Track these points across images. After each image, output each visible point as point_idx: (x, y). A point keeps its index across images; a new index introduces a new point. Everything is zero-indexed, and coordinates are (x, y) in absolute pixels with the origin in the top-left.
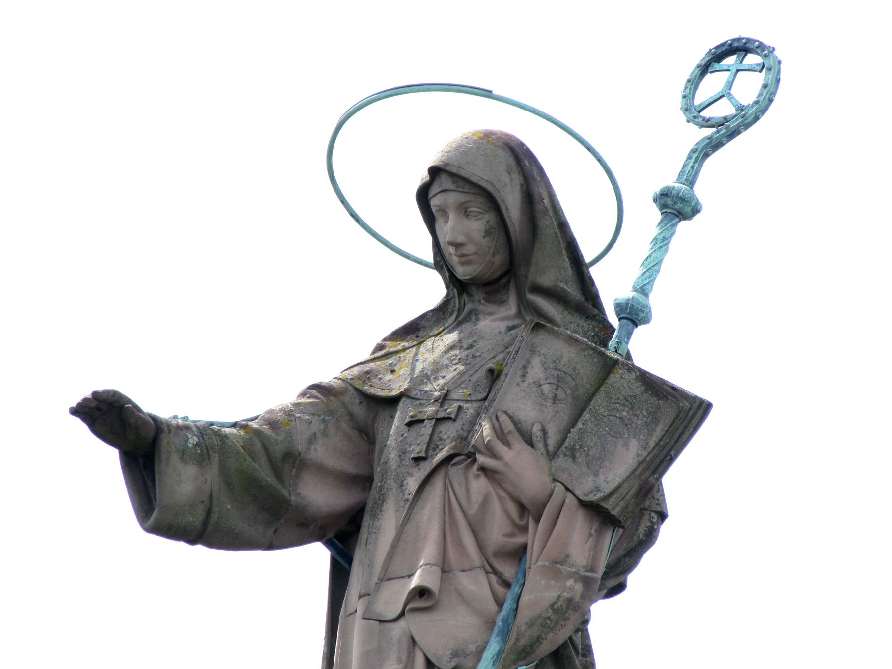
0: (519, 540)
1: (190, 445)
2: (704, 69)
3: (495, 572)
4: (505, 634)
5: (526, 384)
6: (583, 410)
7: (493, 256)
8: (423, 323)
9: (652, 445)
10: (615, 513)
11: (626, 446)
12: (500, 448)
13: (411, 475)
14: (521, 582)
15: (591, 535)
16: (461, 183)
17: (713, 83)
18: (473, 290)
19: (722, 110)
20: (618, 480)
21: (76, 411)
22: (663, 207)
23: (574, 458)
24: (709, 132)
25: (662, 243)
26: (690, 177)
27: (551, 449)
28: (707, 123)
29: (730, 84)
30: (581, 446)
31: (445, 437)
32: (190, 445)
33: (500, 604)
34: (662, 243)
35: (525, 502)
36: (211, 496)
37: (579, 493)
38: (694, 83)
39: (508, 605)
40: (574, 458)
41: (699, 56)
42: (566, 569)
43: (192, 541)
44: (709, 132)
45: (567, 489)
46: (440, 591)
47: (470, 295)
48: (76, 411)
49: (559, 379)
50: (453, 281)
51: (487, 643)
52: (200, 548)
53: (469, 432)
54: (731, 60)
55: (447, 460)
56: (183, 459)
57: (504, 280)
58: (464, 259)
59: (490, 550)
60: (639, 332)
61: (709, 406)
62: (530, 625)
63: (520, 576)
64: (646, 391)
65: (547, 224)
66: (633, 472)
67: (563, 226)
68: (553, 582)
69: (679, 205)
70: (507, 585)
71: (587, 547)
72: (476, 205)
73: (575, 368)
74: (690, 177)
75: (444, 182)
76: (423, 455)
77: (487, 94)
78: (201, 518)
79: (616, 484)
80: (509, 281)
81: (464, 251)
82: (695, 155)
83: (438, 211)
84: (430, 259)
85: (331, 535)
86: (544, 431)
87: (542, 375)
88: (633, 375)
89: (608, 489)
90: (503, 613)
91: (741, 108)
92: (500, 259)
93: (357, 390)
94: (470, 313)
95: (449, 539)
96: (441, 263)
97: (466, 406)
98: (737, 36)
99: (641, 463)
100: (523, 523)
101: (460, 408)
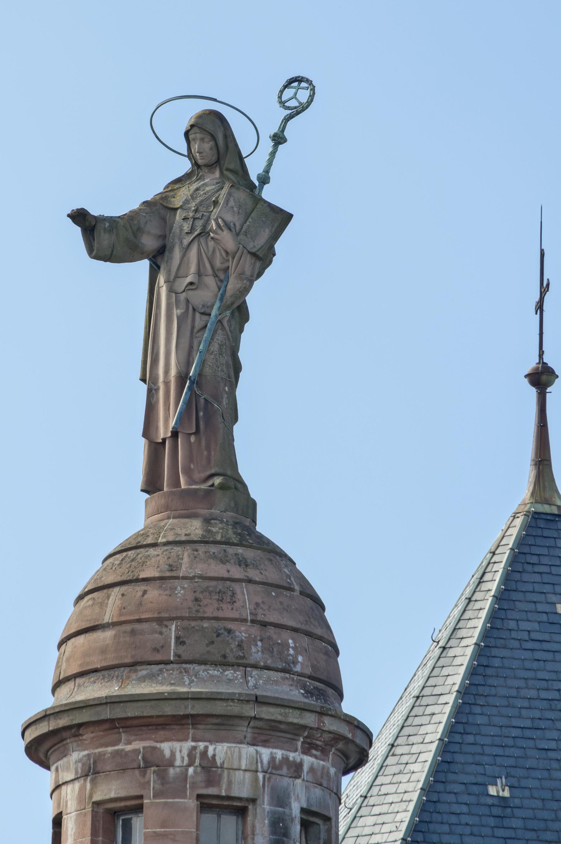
0: (226, 265)
1: (106, 226)
2: (285, 87)
3: (217, 276)
4: (221, 300)
5: (228, 207)
6: (248, 217)
7: (212, 156)
8: (183, 178)
9: (273, 231)
10: (261, 256)
11: (264, 231)
12: (219, 231)
13: (185, 238)
14: (227, 280)
15: (252, 264)
16: (202, 130)
17: (289, 93)
18: (203, 168)
19: (293, 103)
20: (262, 244)
21: (69, 216)
22: (273, 140)
23: (246, 235)
24: (289, 112)
25: (273, 154)
26: (283, 128)
27: (237, 232)
28: (288, 108)
29: (296, 94)
30: (249, 231)
31: (198, 225)
32: (106, 226)
33: (219, 289)
34: (273, 154)
35: (229, 251)
36: (113, 244)
37: (248, 248)
38: (282, 92)
39: (222, 289)
40: (246, 235)
41: (283, 82)
42: (243, 276)
43: (105, 261)
44: (289, 112)
45: (244, 247)
46: (198, 282)
47: (201, 169)
48: (69, 216)
49: (240, 206)
50: (196, 165)
51: (215, 302)
52: (108, 263)
53: (206, 224)
54: (296, 84)
55: (199, 235)
56: (105, 232)
57: (215, 165)
58: (201, 158)
59: (216, 268)
60: (266, 186)
61: (526, 376)
62: (231, 296)
63: (227, 278)
64: (271, 211)
65: (231, 145)
66: (267, 241)
67: (236, 145)
68: (239, 281)
69: (280, 140)
70: (221, 281)
71: (250, 268)
72: (208, 138)
73: (246, 202)
74: (283, 128)
75: (195, 129)
76: (190, 232)
77: (215, 100)
78: (110, 253)
79: (261, 246)
80: (217, 166)
81: (202, 155)
82: (284, 121)
83: (192, 140)
84: (186, 154)
85: (151, 256)
86: (235, 225)
87: (234, 204)
88: (266, 205)
89: (259, 247)
90: (221, 292)
91: (301, 103)
92: (214, 158)
93: (161, 204)
94: (201, 176)
95: (200, 263)
96: (190, 155)
97: (205, 214)
98: (298, 75)
99: (269, 238)
100: (228, 259)
101: (203, 214)
